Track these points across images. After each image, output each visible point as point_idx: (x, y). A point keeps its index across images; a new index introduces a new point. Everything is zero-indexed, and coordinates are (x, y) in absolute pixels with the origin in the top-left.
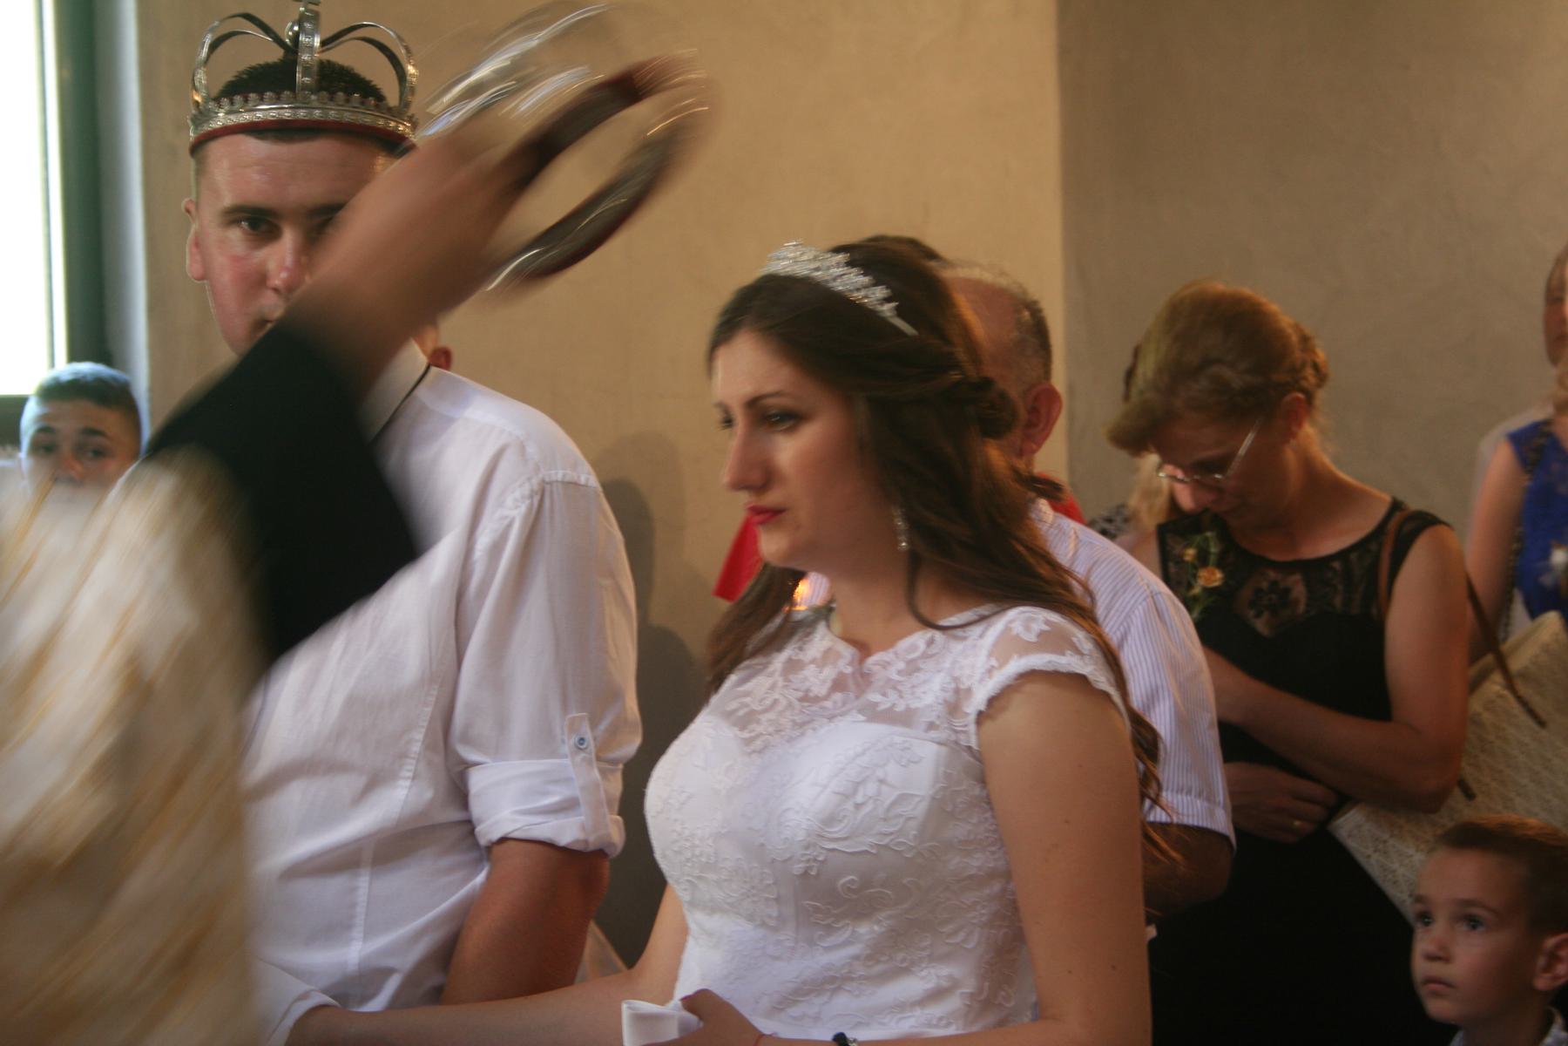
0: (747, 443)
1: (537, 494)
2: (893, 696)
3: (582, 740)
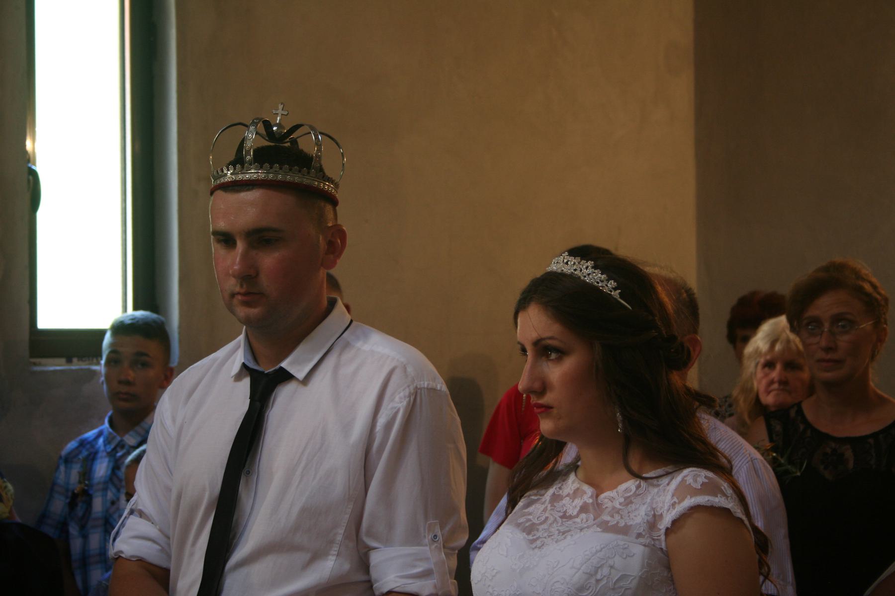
1: (413, 394)
2: (617, 517)
3: (435, 536)
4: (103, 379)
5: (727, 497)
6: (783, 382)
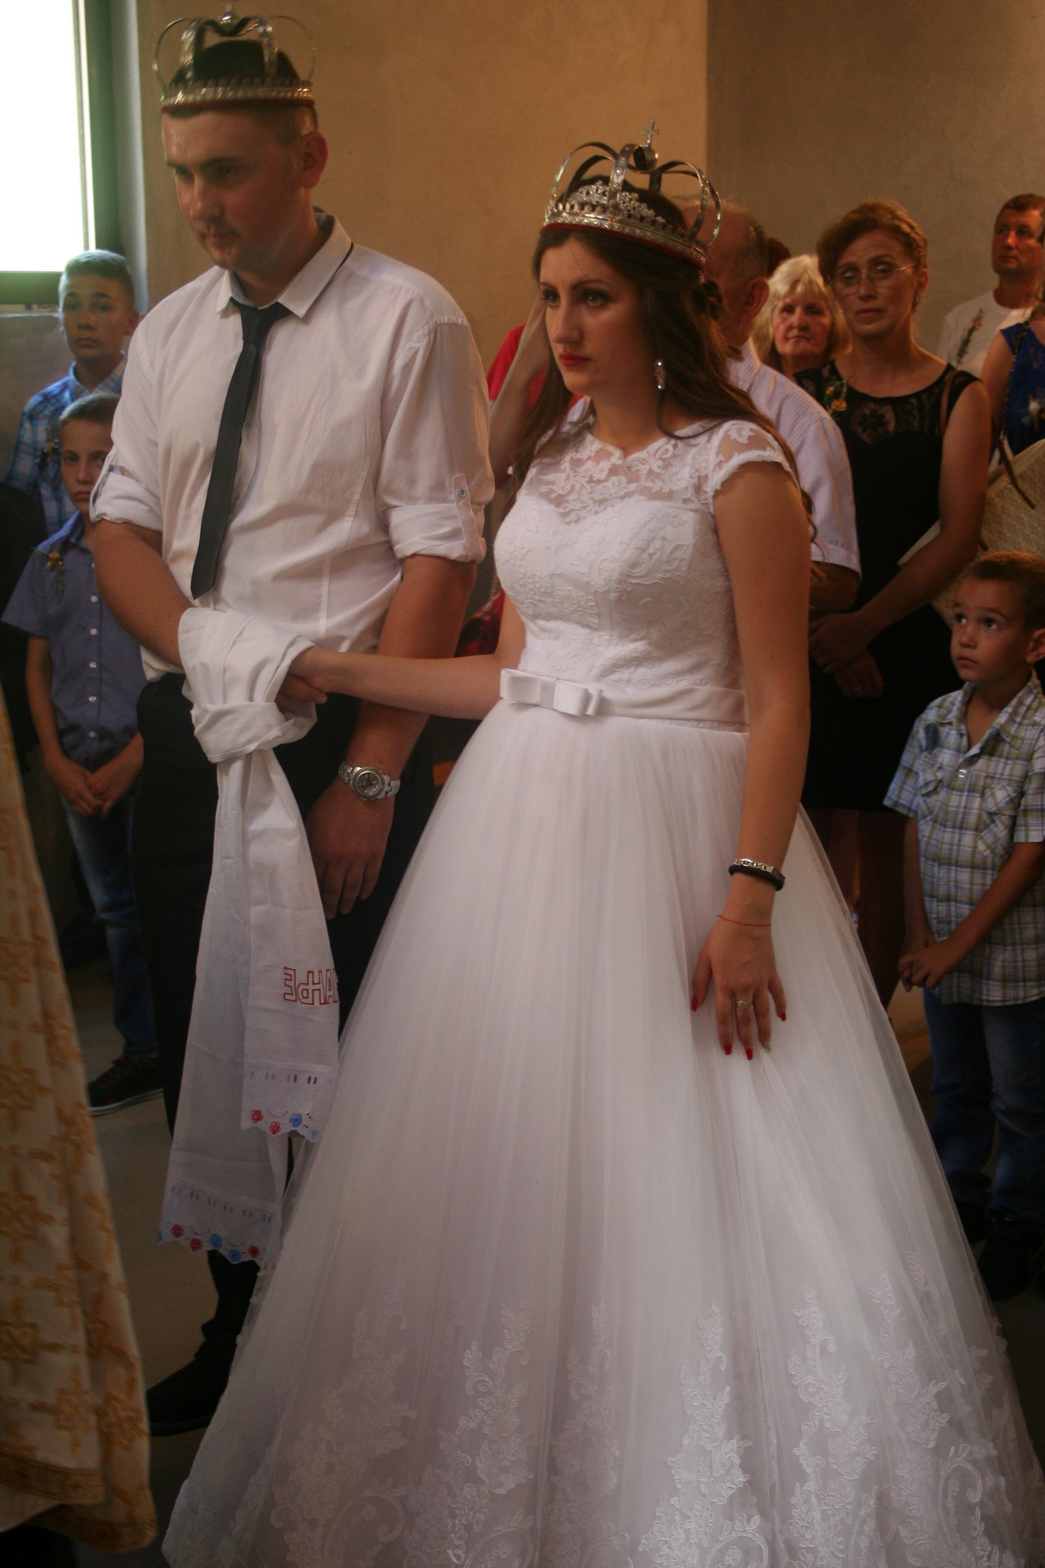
0: (570, 313)
4: (62, 328)
6: (803, 328)
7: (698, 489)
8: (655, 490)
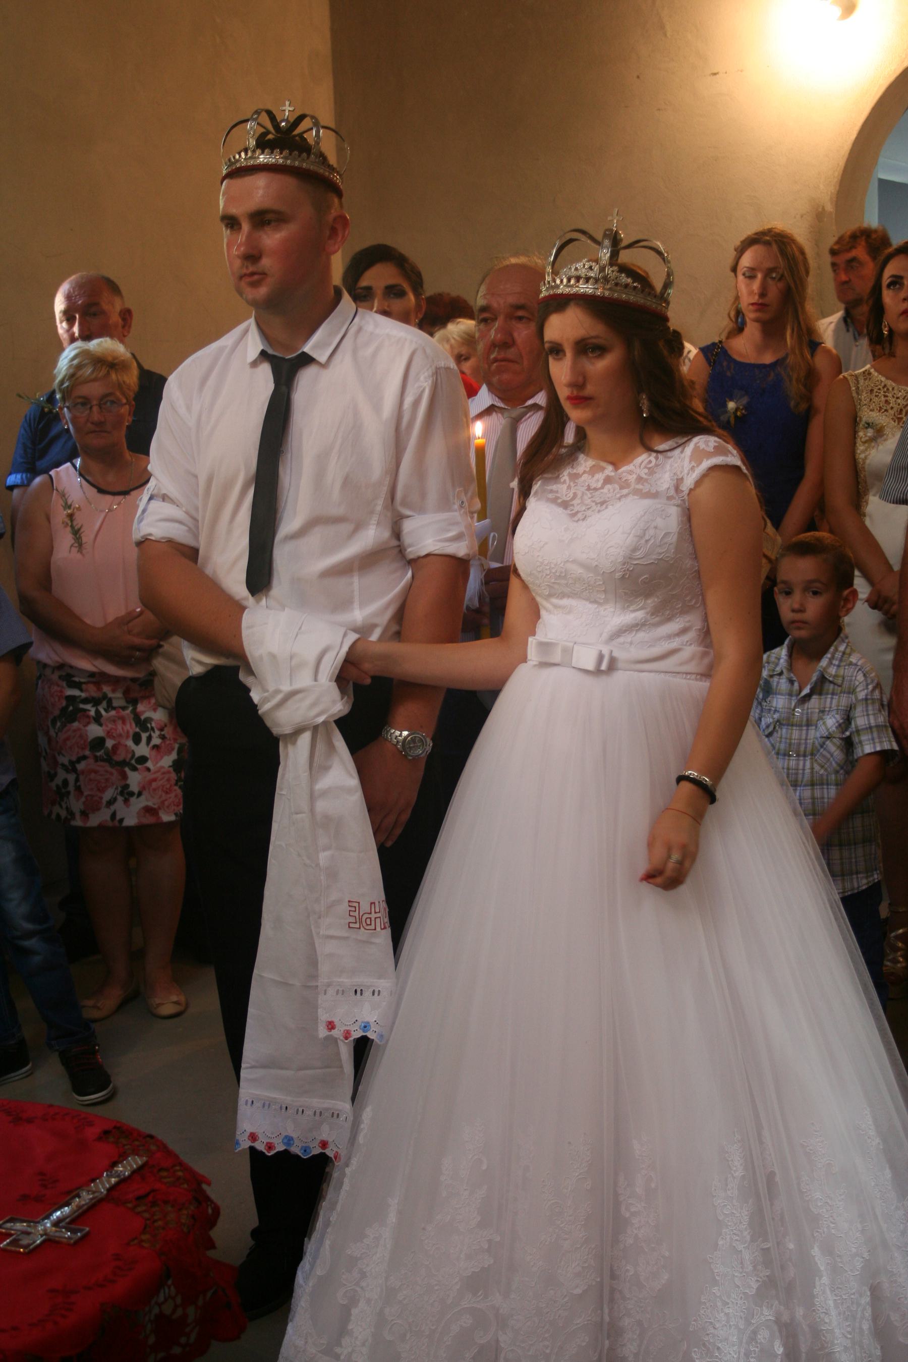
5: (734, 456)
7: (677, 489)
8: (644, 491)
